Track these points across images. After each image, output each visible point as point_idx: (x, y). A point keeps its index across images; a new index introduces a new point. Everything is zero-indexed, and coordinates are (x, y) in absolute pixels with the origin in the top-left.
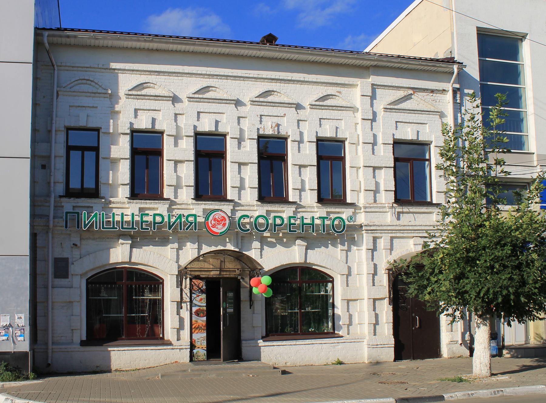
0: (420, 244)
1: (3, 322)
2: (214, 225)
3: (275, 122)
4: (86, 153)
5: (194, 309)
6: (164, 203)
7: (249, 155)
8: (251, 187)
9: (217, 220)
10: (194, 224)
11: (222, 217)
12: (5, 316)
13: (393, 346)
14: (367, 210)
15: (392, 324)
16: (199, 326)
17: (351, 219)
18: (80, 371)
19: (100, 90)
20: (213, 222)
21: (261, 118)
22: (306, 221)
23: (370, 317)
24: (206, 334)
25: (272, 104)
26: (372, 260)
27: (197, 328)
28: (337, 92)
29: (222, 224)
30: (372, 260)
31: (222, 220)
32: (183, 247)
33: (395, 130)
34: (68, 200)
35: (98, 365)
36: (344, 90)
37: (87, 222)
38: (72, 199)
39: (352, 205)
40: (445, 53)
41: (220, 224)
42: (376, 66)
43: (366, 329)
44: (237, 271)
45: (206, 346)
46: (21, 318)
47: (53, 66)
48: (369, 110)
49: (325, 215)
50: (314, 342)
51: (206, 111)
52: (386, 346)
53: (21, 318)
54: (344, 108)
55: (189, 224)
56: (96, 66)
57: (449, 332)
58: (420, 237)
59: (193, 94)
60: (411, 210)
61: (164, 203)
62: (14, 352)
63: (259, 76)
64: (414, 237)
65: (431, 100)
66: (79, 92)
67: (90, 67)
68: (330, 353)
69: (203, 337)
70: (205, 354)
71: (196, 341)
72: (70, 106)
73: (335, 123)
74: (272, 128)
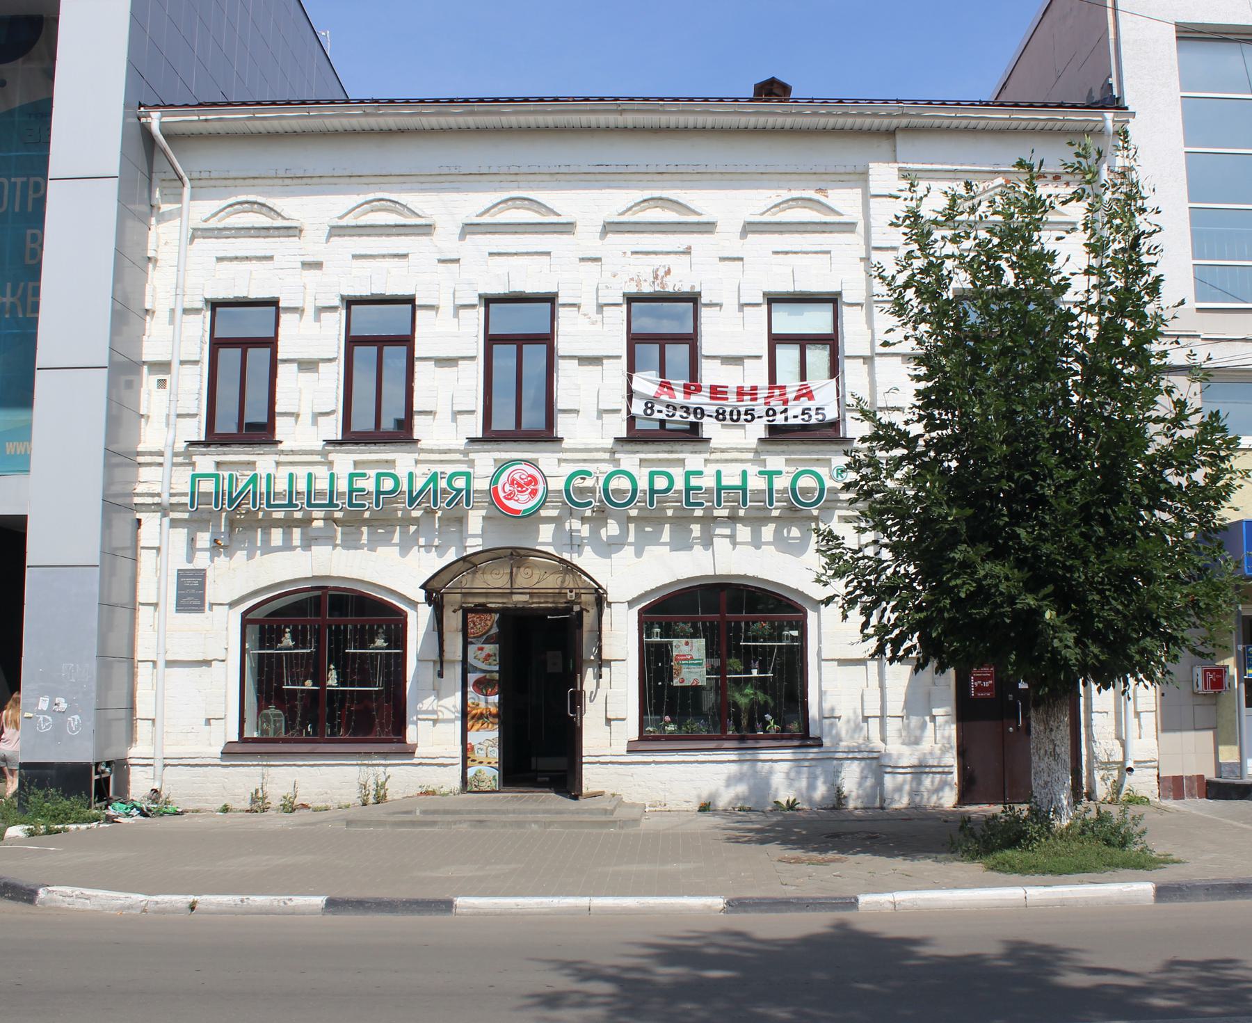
2: (511, 493)
4: (526, 348)
10: (464, 492)
11: (530, 476)
20: (508, 488)
22: (726, 482)
29: (528, 492)
31: (528, 484)
37: (234, 495)
40: (1102, 88)
44: (569, 594)
47: (181, 179)
55: (455, 492)
71: (476, 748)
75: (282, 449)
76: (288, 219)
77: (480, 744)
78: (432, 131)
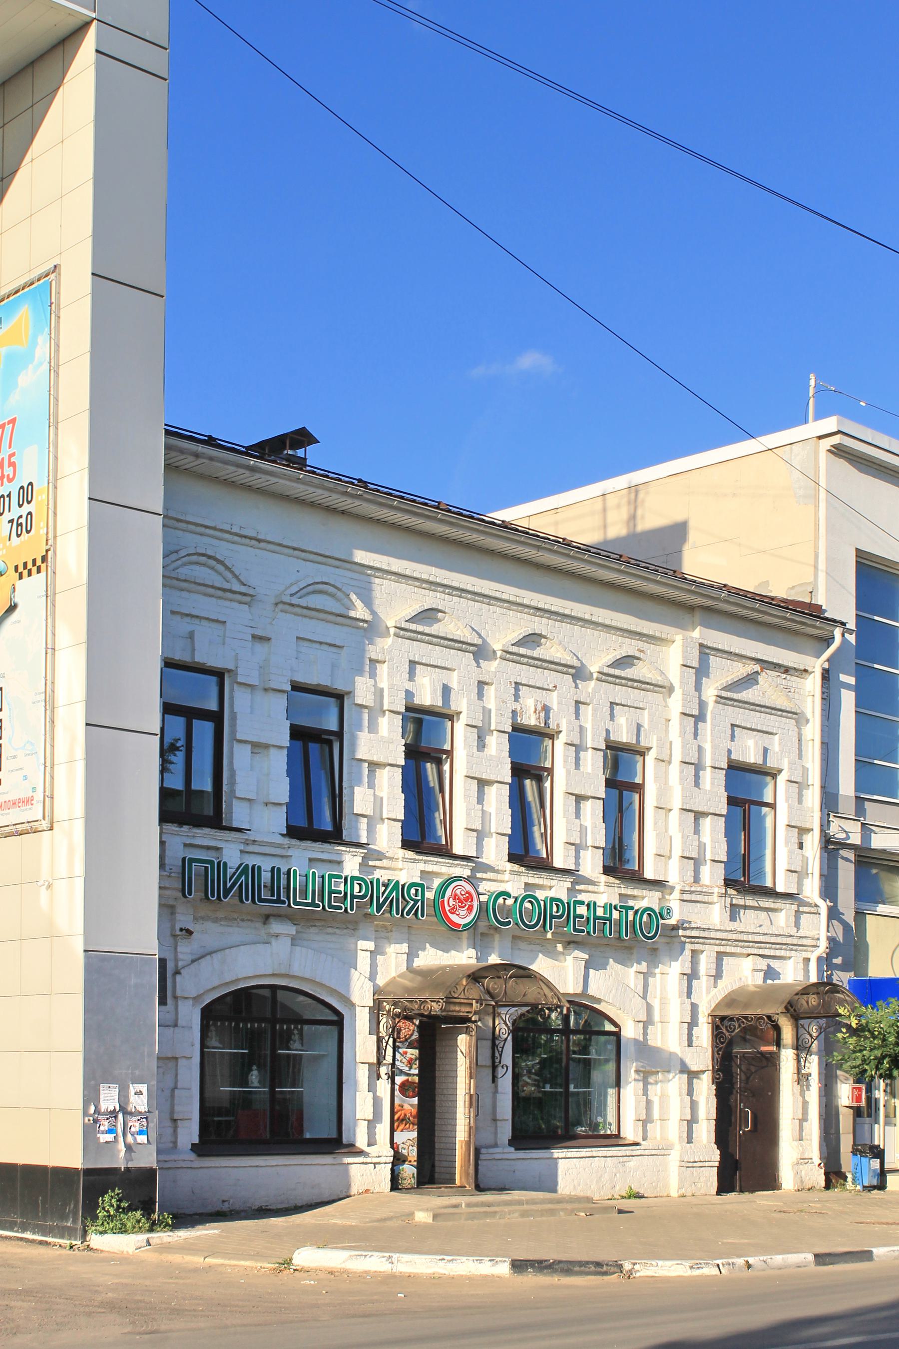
0: (761, 970)
1: (105, 1101)
2: (454, 908)
3: (541, 702)
5: (399, 1080)
6: (355, 852)
7: (498, 766)
8: (499, 832)
9: (459, 898)
10: (419, 903)
11: (468, 892)
12: (109, 1087)
13: (717, 1164)
14: (686, 897)
15: (714, 1122)
16: (405, 1115)
17: (668, 913)
18: (191, 1213)
19: (236, 587)
20: (452, 902)
21: (517, 690)
23: (682, 1108)
24: (416, 1133)
25: (536, 662)
26: (689, 995)
27: (403, 1120)
28: (638, 650)
30: (689, 995)
31: (466, 900)
32: (420, 952)
33: (729, 742)
34: (177, 829)
35: (225, 1199)
36: (649, 648)
37: (229, 885)
38: (185, 828)
39: (657, 884)
41: (463, 907)
42: (708, 609)
43: (674, 1130)
45: (416, 1159)
46: (142, 1094)
48: (694, 697)
49: (615, 901)
50: (595, 1154)
51: (424, 662)
52: (707, 1164)
53: (141, 1093)
54: (652, 687)
55: (412, 902)
56: (227, 527)
57: (796, 1140)
58: (759, 955)
59: (406, 621)
60: (763, 904)
61: (355, 852)
62: (128, 1170)
63: (519, 600)
64: (749, 955)
65: (782, 687)
66: (195, 583)
67: (214, 528)
68: (618, 1175)
69: (411, 1139)
70: (413, 1174)
72: (298, 638)
73: (444, 677)
74: (535, 712)
75: (852, 913)
76: (245, 585)
77: (403, 1143)
78: (378, 521)
